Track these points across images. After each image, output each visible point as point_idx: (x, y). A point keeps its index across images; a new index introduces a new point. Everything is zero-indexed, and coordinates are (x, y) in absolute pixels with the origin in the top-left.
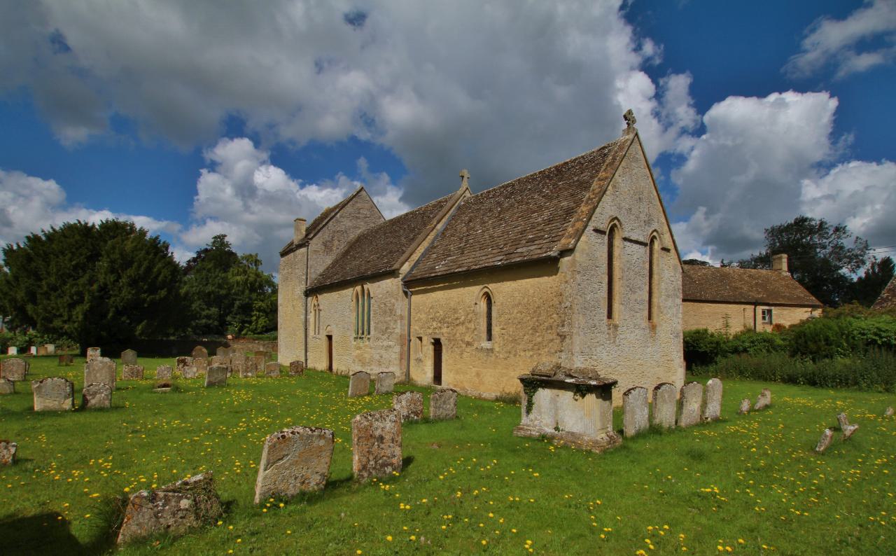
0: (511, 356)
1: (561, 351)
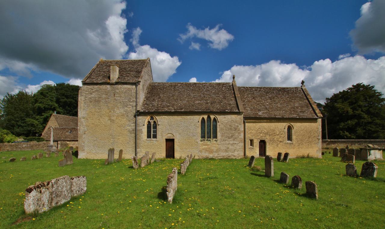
0: (301, 145)
1: (318, 143)
